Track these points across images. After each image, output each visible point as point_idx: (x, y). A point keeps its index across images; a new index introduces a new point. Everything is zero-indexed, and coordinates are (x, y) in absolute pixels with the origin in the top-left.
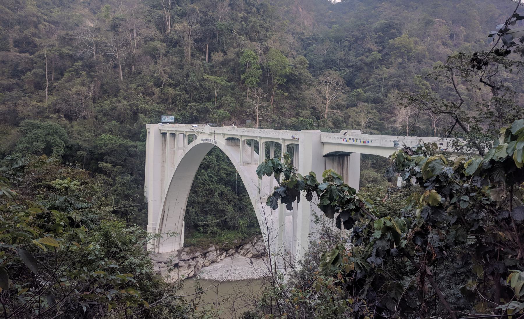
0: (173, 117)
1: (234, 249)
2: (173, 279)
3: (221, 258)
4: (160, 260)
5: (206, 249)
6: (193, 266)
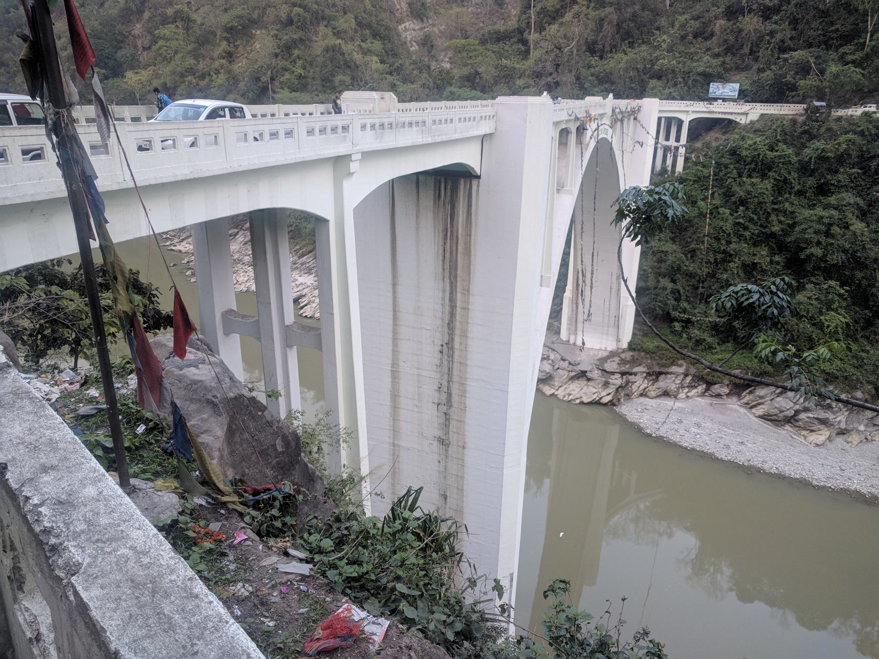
0: (737, 86)
1: (728, 385)
2: (569, 395)
3: (689, 394)
4: (566, 357)
5: (664, 366)
6: (613, 386)
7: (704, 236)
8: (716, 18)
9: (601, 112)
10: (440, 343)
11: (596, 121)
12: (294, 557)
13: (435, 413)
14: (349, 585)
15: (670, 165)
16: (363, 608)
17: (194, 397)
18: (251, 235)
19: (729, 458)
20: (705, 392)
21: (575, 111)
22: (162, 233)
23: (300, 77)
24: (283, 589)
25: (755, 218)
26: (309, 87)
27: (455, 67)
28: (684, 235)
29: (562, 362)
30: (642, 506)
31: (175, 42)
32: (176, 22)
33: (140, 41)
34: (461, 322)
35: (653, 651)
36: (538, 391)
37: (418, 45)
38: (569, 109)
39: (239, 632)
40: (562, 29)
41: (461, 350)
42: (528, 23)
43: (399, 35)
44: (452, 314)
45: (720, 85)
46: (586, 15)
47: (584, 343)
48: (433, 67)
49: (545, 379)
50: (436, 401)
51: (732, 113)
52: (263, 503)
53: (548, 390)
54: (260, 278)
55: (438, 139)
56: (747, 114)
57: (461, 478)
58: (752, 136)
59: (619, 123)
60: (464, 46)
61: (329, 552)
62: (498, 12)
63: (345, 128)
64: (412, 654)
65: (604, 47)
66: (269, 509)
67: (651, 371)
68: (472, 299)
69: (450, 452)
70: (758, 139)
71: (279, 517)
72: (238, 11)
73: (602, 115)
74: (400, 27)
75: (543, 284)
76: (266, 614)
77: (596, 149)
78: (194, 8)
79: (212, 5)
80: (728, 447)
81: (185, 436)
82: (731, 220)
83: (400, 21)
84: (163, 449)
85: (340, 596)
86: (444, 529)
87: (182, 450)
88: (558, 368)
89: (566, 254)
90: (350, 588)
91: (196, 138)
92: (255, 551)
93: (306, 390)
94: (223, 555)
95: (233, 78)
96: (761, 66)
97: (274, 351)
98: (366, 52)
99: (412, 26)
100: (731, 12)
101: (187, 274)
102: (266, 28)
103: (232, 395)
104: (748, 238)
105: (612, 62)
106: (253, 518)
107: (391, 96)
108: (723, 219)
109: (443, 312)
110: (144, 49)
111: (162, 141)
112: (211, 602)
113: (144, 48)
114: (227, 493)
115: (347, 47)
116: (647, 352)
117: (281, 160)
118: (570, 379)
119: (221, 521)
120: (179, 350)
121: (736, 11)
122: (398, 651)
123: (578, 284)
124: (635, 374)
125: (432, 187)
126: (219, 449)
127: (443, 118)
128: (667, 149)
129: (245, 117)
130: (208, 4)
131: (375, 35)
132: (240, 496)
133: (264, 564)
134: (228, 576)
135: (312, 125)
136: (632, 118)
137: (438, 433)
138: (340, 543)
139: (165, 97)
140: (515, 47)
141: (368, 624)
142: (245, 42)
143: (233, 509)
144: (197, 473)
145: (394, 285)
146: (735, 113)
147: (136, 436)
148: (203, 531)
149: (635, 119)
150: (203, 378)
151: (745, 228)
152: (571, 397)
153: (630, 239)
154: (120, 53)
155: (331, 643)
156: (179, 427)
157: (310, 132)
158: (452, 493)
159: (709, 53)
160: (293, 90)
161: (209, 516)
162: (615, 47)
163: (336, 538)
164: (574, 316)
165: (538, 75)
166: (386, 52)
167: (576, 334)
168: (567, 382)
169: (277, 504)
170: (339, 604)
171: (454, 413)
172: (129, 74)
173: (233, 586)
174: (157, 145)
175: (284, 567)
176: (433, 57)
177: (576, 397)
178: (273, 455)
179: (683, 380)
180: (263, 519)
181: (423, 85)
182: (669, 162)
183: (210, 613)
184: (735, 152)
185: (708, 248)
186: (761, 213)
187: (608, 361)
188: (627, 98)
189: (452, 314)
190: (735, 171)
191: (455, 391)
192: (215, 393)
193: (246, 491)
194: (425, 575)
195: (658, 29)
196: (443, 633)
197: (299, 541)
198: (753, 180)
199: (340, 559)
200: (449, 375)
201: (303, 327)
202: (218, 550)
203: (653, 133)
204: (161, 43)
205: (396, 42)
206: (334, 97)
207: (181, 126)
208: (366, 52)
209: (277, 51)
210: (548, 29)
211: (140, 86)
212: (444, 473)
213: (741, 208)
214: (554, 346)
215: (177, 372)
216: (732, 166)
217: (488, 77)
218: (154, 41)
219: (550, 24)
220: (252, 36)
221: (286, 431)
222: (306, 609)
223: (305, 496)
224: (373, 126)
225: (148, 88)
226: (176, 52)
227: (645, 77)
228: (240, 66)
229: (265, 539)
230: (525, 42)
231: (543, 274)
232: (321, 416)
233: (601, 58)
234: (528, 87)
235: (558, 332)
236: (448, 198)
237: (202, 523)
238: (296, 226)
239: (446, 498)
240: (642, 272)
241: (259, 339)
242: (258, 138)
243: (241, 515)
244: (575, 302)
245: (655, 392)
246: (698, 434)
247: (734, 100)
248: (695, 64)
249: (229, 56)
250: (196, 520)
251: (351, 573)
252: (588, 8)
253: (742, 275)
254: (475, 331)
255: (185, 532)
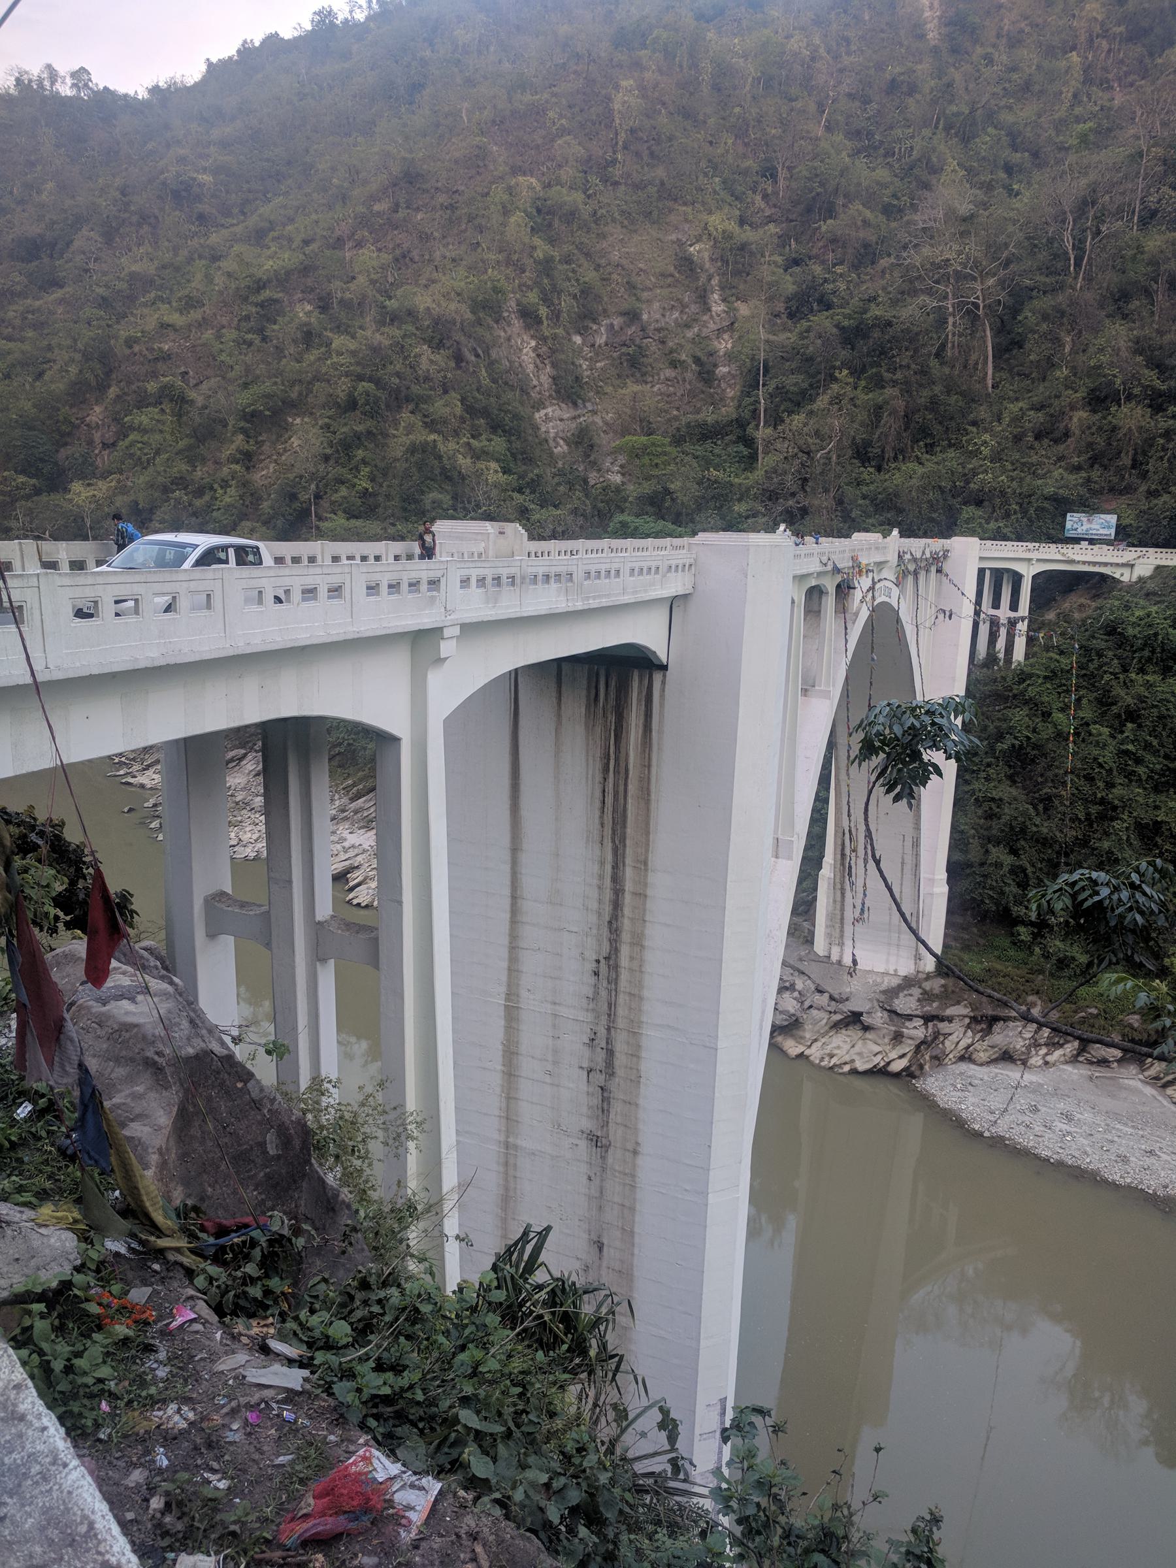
0: (1112, 519)
2: (831, 1056)
3: (1048, 1058)
6: (910, 1042)
7: (1066, 773)
8: (1073, 408)
9: (879, 558)
10: (595, 957)
11: (870, 575)
12: (278, 1355)
13: (583, 1086)
14: (375, 1411)
15: (1003, 650)
16: (395, 1455)
17: (124, 1053)
18: (264, 761)
19: (1128, 1180)
20: (1078, 1055)
21: (833, 557)
22: (116, 755)
23: (365, 493)
24: (251, 1416)
25: (1155, 743)
26: (380, 510)
27: (630, 481)
28: (1030, 771)
29: (817, 996)
30: (970, 1272)
31: (158, 437)
32: (161, 403)
33: (99, 434)
34: (632, 919)
35: (917, 1551)
36: (774, 1047)
37: (568, 444)
38: (823, 554)
39: (83, 1482)
40: (812, 422)
41: (631, 970)
42: (755, 413)
43: (536, 428)
44: (617, 905)
45: (1083, 517)
46: (852, 399)
47: (855, 962)
48: (593, 478)
49: (787, 1027)
50: (585, 1065)
51: (1106, 564)
52: (232, 1251)
53: (793, 1048)
54: (277, 834)
55: (594, 604)
56: (1132, 566)
57: (629, 1209)
58: (1142, 602)
59: (910, 578)
60: (645, 447)
61: (346, 1346)
62: (703, 392)
63: (434, 583)
64: (479, 1549)
65: (883, 451)
66: (241, 1263)
67: (978, 1014)
68: (652, 878)
69: (610, 1160)
70: (1154, 609)
71: (259, 1278)
72: (267, 387)
73: (880, 565)
74: (537, 415)
75: (780, 855)
76: (215, 1465)
77: (870, 625)
78: (192, 382)
79: (224, 378)
80: (1125, 1160)
81: (99, 1128)
82: (1112, 746)
83: (539, 405)
84: (59, 1149)
85: (355, 1432)
86: (587, 1308)
87: (92, 1153)
88: (811, 1007)
89: (821, 801)
90: (377, 1417)
91: (174, 598)
92: (207, 1343)
93: (353, 1039)
94: (149, 1349)
95: (252, 495)
96: (1153, 487)
97: (293, 968)
98: (478, 455)
99: (558, 413)
100: (1098, 398)
101: (152, 826)
102: (311, 414)
103: (191, 1051)
104: (1144, 777)
105: (897, 475)
106: (211, 1280)
107: (516, 531)
108: (1098, 743)
109: (600, 901)
110: (105, 446)
111: (117, 602)
112: (44, 1429)
113: (104, 444)
114: (167, 1232)
115: (448, 447)
117: (319, 635)
118: (831, 1028)
119: (151, 1285)
120: (96, 973)
121: (1106, 397)
122: (452, 1542)
123: (843, 855)
124: (950, 1019)
125: (585, 682)
126: (160, 1151)
127: (603, 568)
128: (994, 623)
129: (261, 563)
130: (216, 376)
131: (496, 427)
132: (192, 1236)
133: (221, 1367)
134: (153, 1390)
135: (377, 577)
136: (933, 569)
137: (587, 1124)
138: (363, 1330)
139: (131, 528)
140: (732, 449)
141: (403, 1487)
142: (274, 437)
143: (176, 1263)
144: (117, 1193)
145: (515, 849)
146: (1111, 564)
147: (13, 1122)
148: (116, 1303)
149: (939, 571)
150: (142, 1021)
151: (1139, 761)
152: (834, 1061)
153: (883, 789)
154: (63, 453)
155: (329, 1524)
156: (90, 1110)
157: (372, 589)
158: (612, 1240)
159: (1063, 464)
160: (352, 515)
161: (130, 1275)
162: (902, 451)
163: (360, 1320)
164: (838, 912)
165: (772, 496)
166: (513, 455)
167: (841, 945)
168: (827, 1033)
169: (257, 1253)
170: (352, 1448)
171: (618, 1088)
172: (77, 486)
173: (159, 1409)
174: (107, 608)
175: (255, 1375)
176: (593, 464)
177: (843, 1060)
178: (259, 1161)
179: (1036, 1032)
180: (229, 1283)
181: (575, 512)
182: (1001, 644)
183: (40, 1447)
184: (1115, 629)
185: (1073, 795)
186: (1164, 733)
187: (901, 995)
188: (925, 535)
189: (617, 905)
190: (1116, 661)
191: (620, 1047)
192: (161, 1047)
193: (203, 1229)
194: (521, 1395)
195: (974, 423)
196: (541, 1509)
197: (291, 1325)
198: (1148, 678)
199: (362, 1360)
200: (609, 1015)
201: (349, 926)
202: (139, 1340)
203: (973, 594)
204: (132, 437)
205: (530, 438)
206: (421, 528)
207: (151, 578)
208: (478, 455)
209: (328, 451)
210: (787, 421)
211: (93, 506)
212: (599, 1200)
213: (1129, 725)
214: (803, 966)
215: (97, 1008)
216: (1110, 654)
217: (685, 499)
218: (123, 433)
219: (790, 413)
220: (287, 427)
221: (286, 1119)
222: (290, 1457)
223: (310, 1238)
224: (481, 581)
225: (106, 509)
226: (158, 452)
227: (955, 502)
228: (264, 475)
229: (227, 1319)
230: (749, 442)
231: (780, 837)
232: (369, 1089)
233: (879, 469)
234: (754, 516)
235: (809, 941)
236: (612, 702)
237: (116, 1288)
238: (349, 744)
239: (601, 1249)
240: (957, 836)
241: (268, 945)
242: (283, 597)
243: (190, 1273)
244: (839, 886)
245: (987, 1054)
246: (1069, 1133)
247: (1108, 543)
248: (1040, 482)
249: (248, 459)
250: (104, 1282)
251: (379, 1387)
252: (856, 388)
253: (1136, 843)
254: (657, 936)
255: (82, 1306)
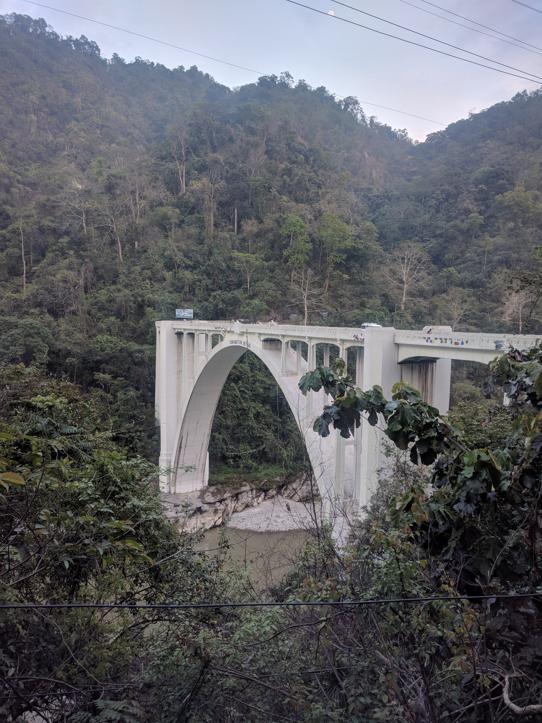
0: (192, 311)
2: (194, 528)
5: (237, 489)
45: (182, 310)
116: (222, 484)
